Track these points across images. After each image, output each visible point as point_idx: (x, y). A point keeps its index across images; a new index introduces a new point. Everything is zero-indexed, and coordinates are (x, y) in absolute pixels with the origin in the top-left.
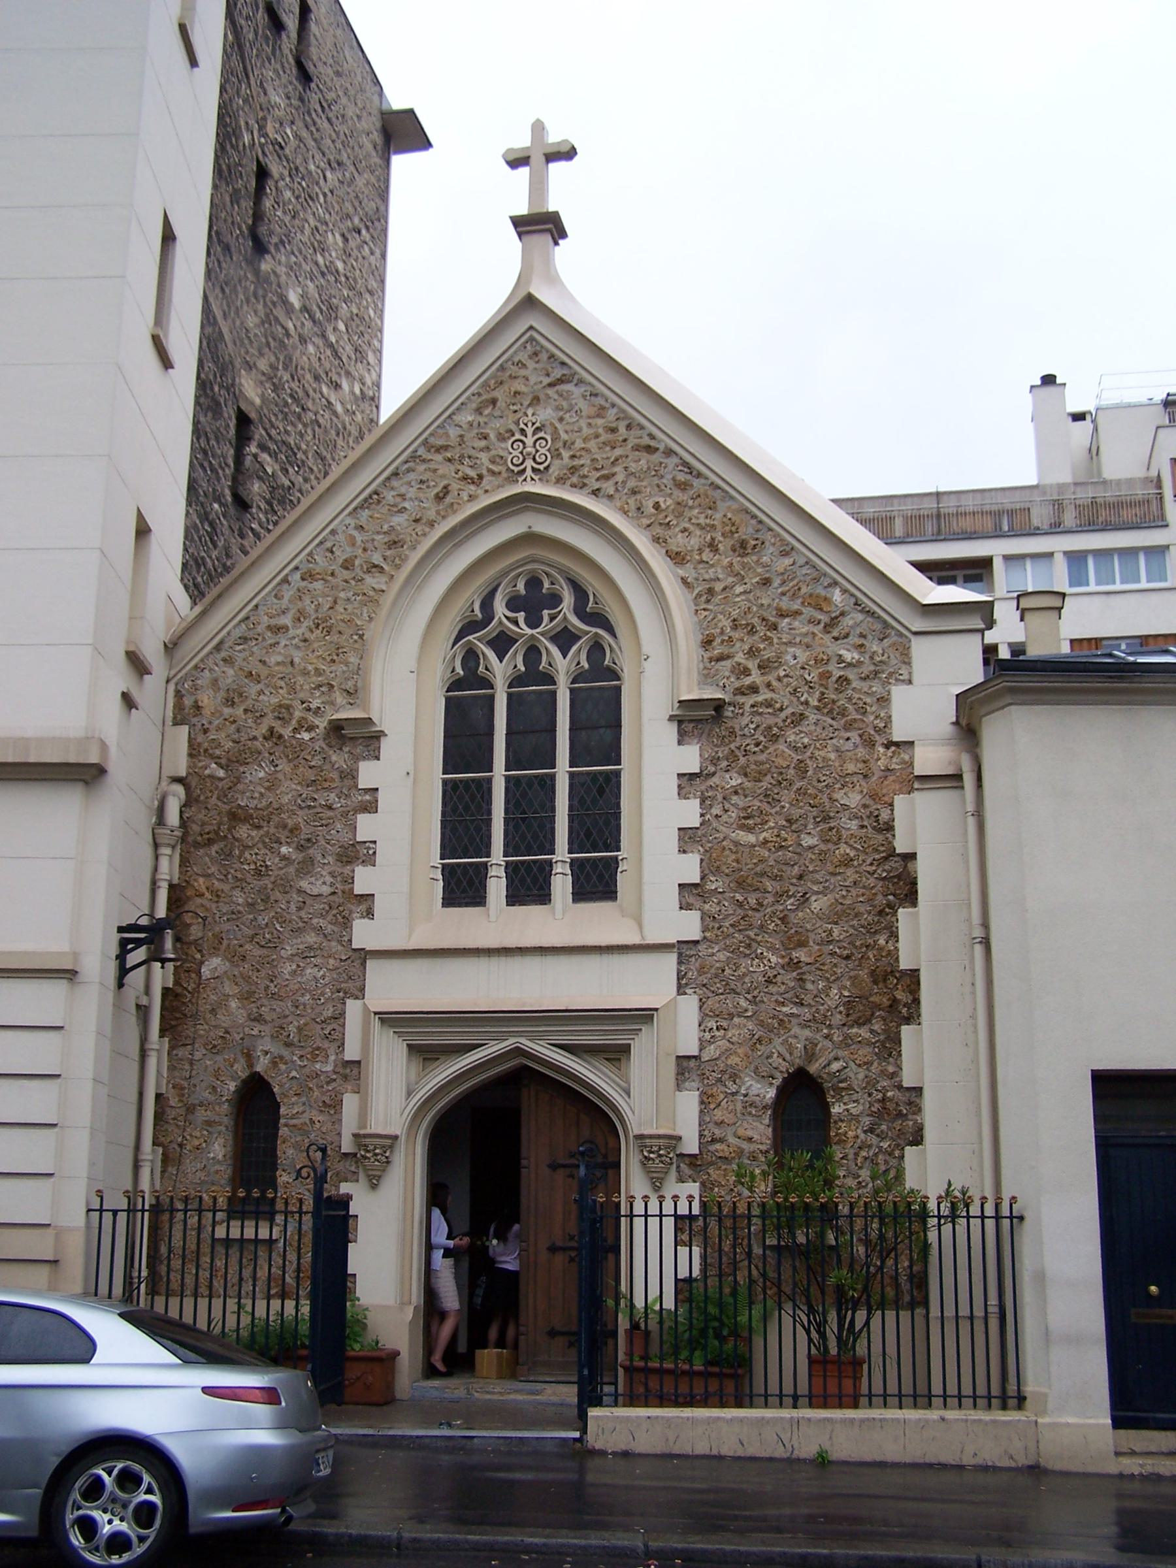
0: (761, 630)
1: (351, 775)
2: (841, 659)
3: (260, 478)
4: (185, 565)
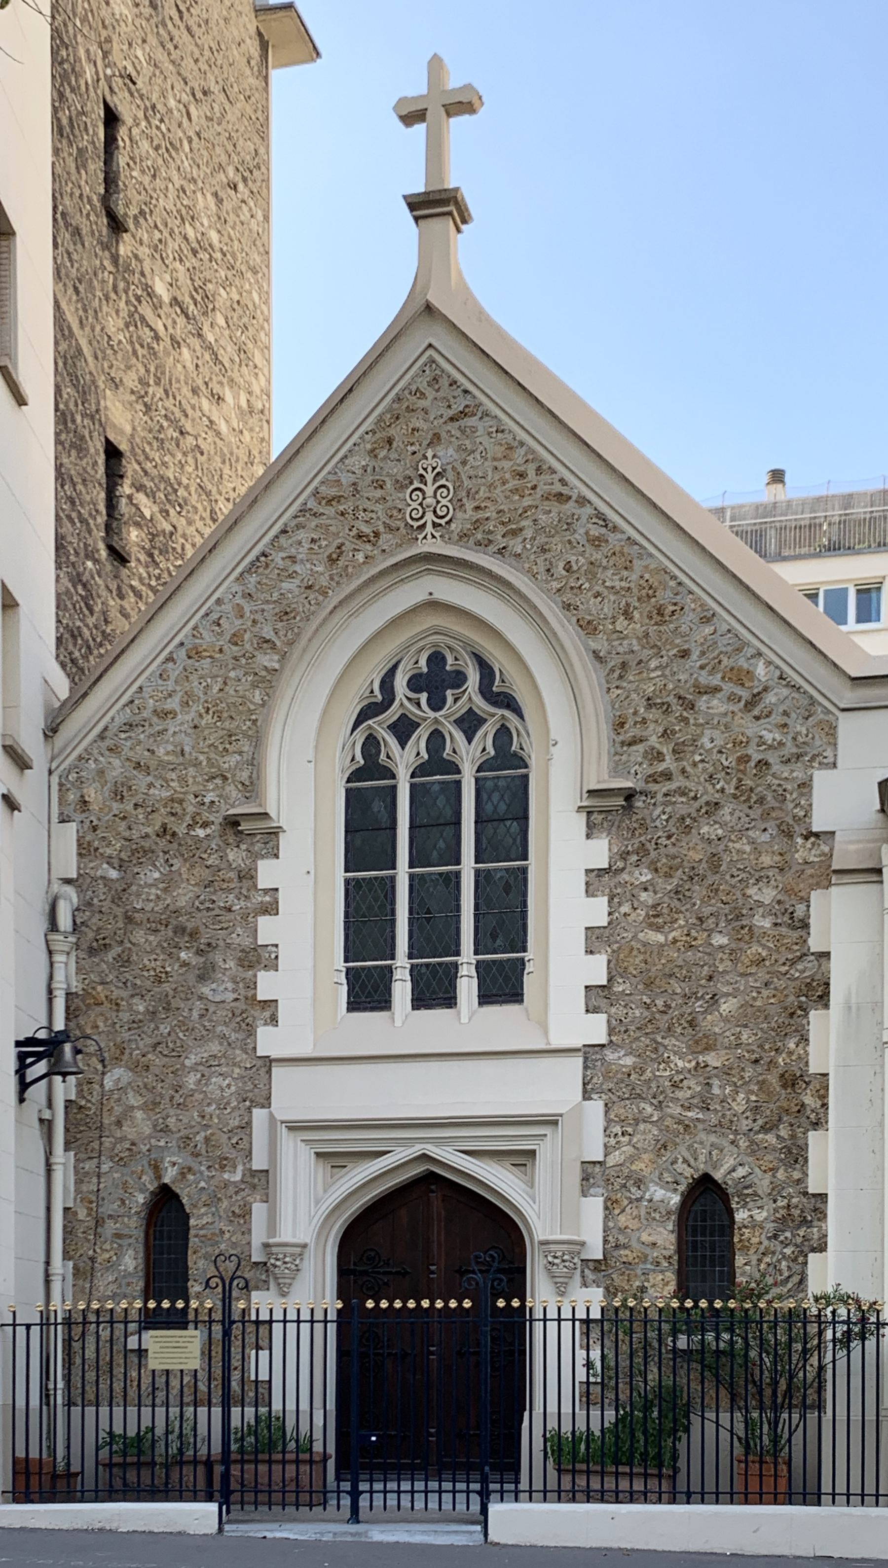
0: (677, 709)
1: (248, 876)
2: (761, 742)
3: (137, 525)
4: (59, 640)
